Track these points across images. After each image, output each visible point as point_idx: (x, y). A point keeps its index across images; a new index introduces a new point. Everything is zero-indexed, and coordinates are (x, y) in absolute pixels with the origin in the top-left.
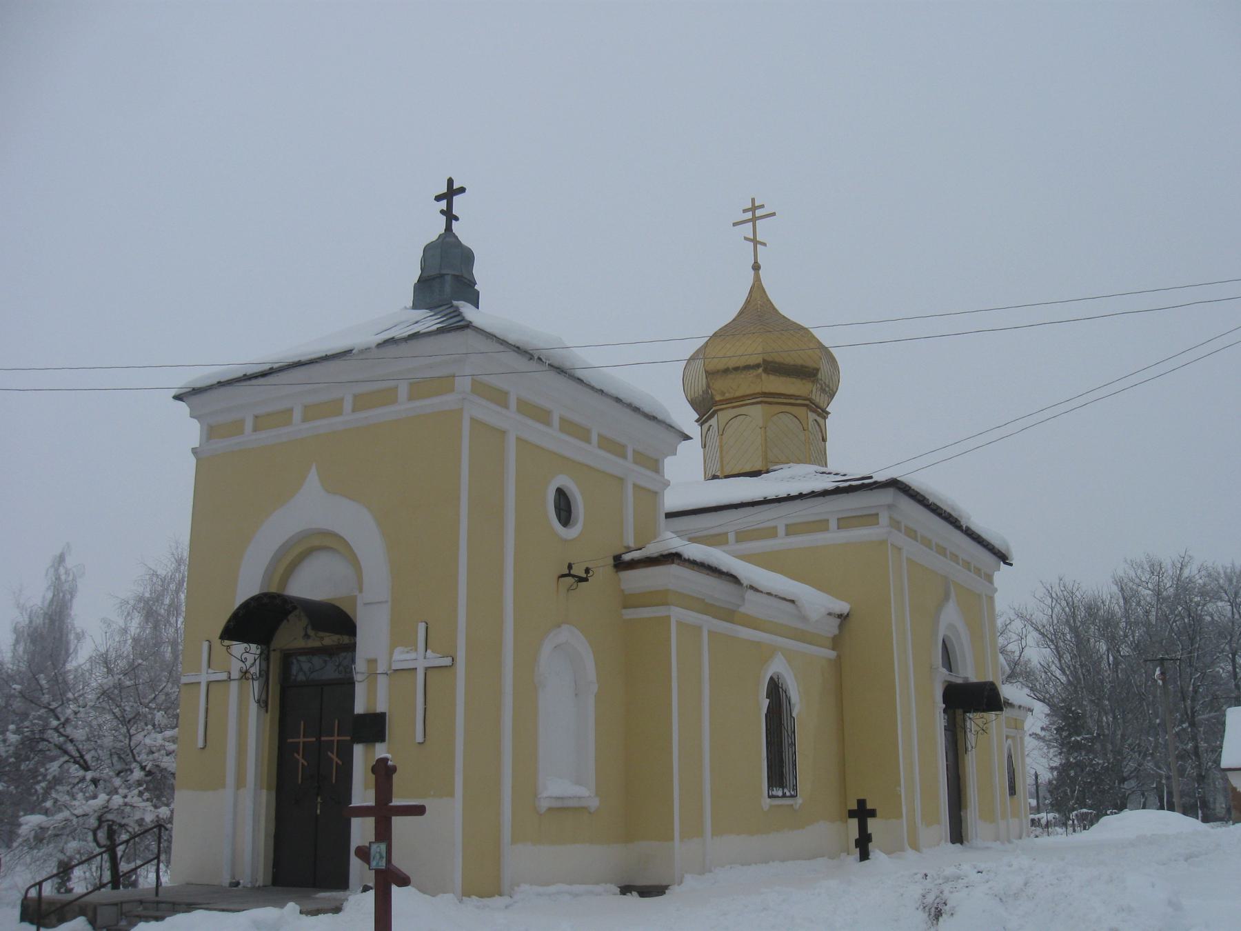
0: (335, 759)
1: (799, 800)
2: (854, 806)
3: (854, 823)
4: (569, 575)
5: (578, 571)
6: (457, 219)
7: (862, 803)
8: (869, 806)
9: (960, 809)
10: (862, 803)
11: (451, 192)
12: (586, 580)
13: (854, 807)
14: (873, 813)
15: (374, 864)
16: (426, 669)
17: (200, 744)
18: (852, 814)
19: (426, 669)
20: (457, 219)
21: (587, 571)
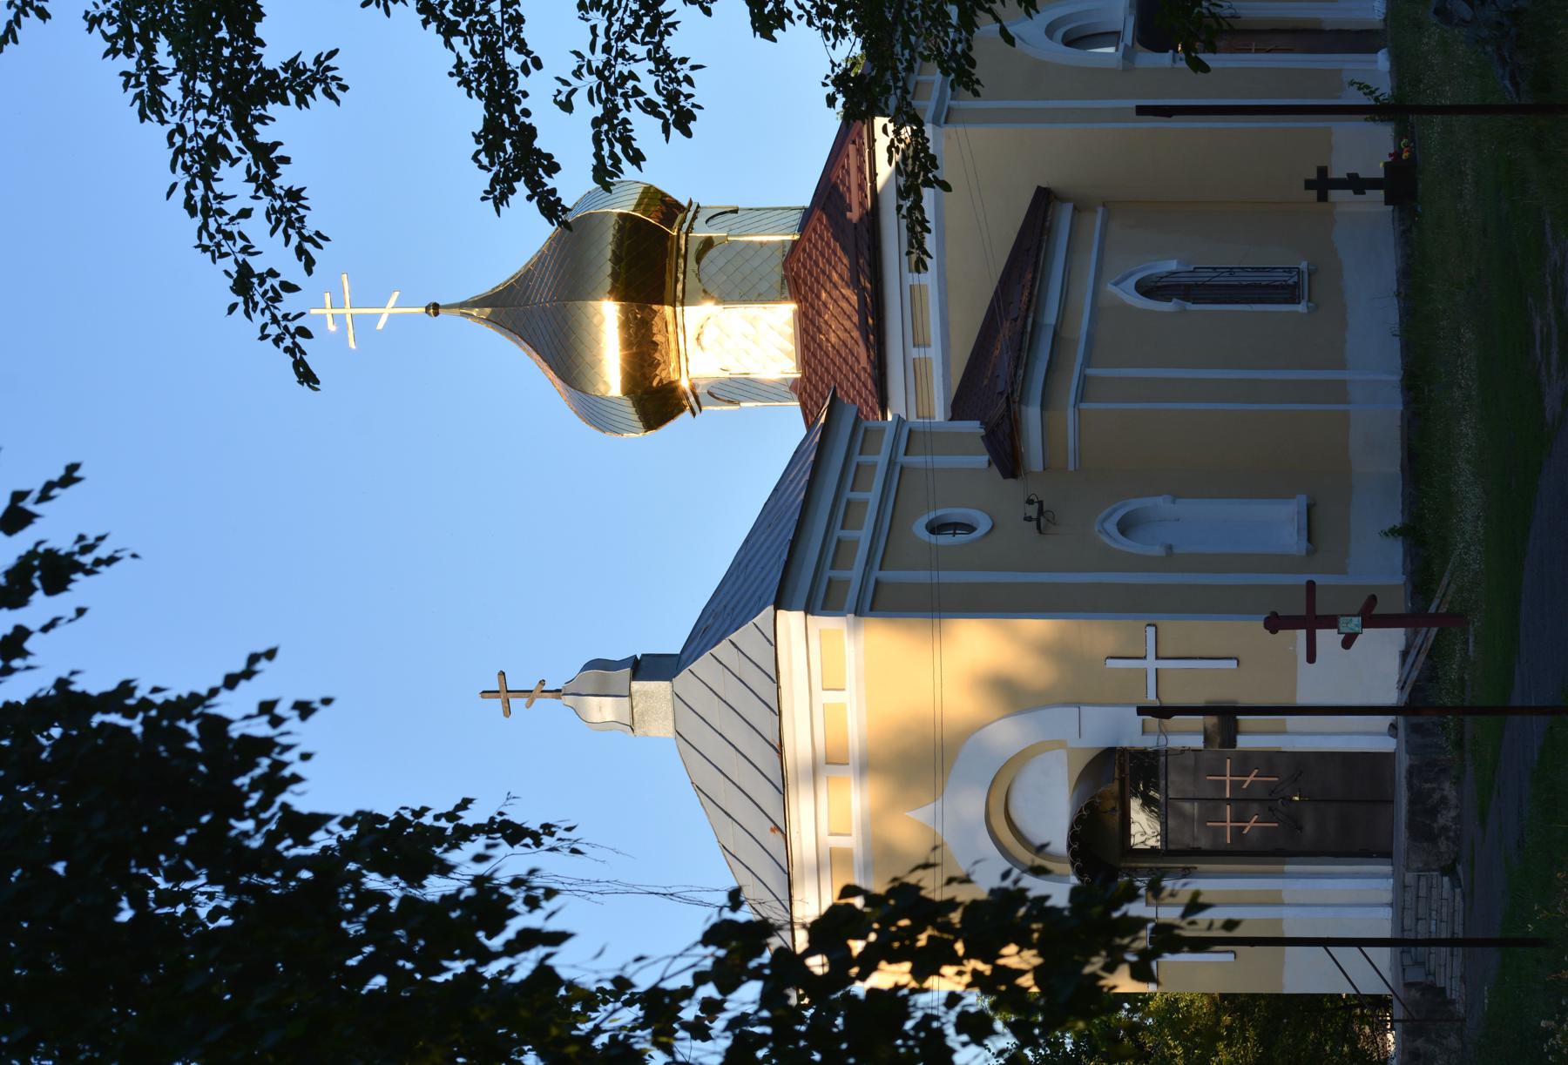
0: (1251, 778)
1: (1303, 265)
2: (1313, 175)
3: (1334, 195)
4: (1038, 520)
5: (1033, 511)
6: (16, 41)
7: (1309, 185)
8: (1313, 176)
9: (1322, 32)
10: (1309, 185)
11: (503, 693)
12: (1041, 503)
13: (1313, 194)
14: (1322, 171)
15: (1357, 629)
16: (1157, 658)
17: (1233, 664)
18: (1323, 197)
19: (1157, 658)
20: (16, 41)
21: (1030, 502)
